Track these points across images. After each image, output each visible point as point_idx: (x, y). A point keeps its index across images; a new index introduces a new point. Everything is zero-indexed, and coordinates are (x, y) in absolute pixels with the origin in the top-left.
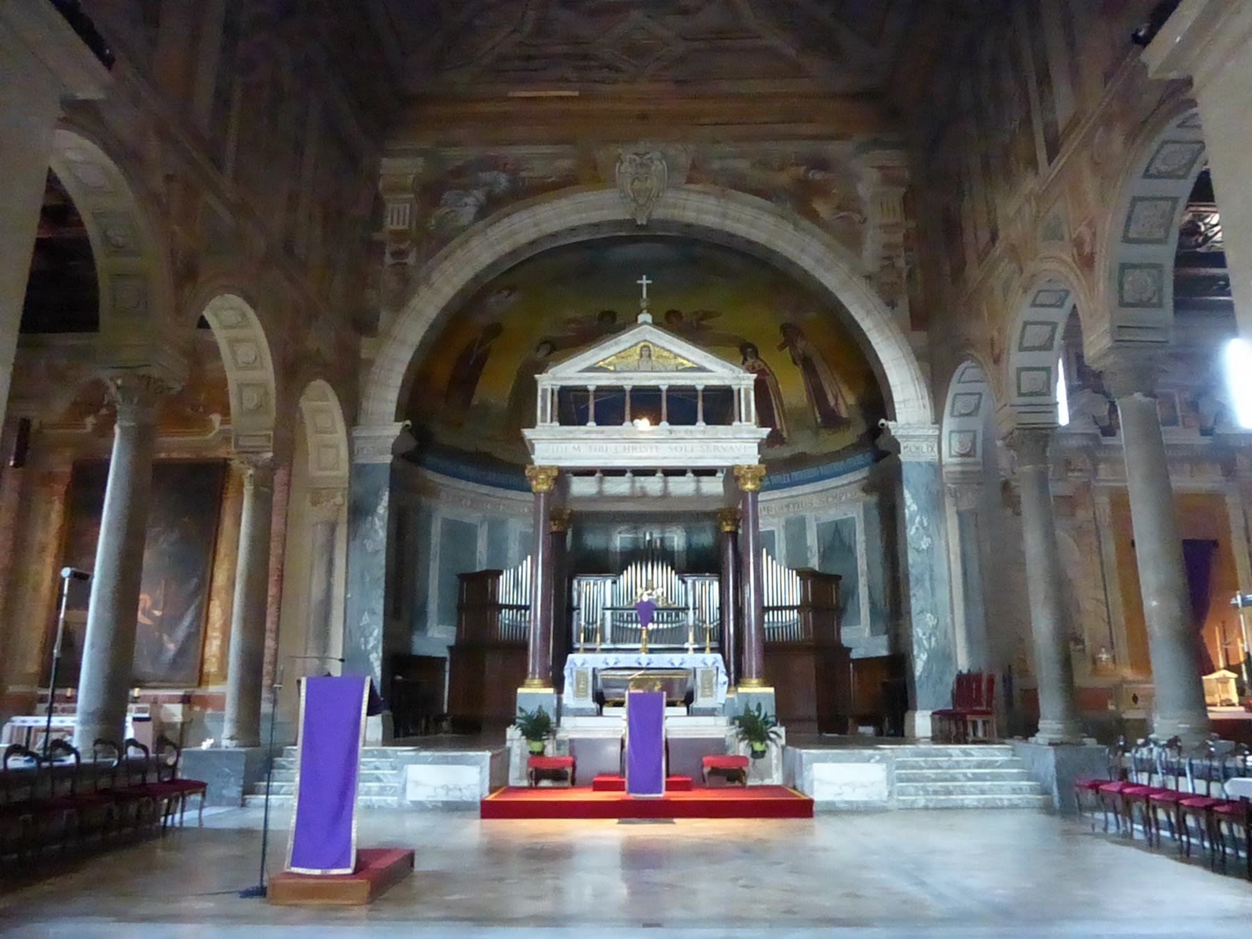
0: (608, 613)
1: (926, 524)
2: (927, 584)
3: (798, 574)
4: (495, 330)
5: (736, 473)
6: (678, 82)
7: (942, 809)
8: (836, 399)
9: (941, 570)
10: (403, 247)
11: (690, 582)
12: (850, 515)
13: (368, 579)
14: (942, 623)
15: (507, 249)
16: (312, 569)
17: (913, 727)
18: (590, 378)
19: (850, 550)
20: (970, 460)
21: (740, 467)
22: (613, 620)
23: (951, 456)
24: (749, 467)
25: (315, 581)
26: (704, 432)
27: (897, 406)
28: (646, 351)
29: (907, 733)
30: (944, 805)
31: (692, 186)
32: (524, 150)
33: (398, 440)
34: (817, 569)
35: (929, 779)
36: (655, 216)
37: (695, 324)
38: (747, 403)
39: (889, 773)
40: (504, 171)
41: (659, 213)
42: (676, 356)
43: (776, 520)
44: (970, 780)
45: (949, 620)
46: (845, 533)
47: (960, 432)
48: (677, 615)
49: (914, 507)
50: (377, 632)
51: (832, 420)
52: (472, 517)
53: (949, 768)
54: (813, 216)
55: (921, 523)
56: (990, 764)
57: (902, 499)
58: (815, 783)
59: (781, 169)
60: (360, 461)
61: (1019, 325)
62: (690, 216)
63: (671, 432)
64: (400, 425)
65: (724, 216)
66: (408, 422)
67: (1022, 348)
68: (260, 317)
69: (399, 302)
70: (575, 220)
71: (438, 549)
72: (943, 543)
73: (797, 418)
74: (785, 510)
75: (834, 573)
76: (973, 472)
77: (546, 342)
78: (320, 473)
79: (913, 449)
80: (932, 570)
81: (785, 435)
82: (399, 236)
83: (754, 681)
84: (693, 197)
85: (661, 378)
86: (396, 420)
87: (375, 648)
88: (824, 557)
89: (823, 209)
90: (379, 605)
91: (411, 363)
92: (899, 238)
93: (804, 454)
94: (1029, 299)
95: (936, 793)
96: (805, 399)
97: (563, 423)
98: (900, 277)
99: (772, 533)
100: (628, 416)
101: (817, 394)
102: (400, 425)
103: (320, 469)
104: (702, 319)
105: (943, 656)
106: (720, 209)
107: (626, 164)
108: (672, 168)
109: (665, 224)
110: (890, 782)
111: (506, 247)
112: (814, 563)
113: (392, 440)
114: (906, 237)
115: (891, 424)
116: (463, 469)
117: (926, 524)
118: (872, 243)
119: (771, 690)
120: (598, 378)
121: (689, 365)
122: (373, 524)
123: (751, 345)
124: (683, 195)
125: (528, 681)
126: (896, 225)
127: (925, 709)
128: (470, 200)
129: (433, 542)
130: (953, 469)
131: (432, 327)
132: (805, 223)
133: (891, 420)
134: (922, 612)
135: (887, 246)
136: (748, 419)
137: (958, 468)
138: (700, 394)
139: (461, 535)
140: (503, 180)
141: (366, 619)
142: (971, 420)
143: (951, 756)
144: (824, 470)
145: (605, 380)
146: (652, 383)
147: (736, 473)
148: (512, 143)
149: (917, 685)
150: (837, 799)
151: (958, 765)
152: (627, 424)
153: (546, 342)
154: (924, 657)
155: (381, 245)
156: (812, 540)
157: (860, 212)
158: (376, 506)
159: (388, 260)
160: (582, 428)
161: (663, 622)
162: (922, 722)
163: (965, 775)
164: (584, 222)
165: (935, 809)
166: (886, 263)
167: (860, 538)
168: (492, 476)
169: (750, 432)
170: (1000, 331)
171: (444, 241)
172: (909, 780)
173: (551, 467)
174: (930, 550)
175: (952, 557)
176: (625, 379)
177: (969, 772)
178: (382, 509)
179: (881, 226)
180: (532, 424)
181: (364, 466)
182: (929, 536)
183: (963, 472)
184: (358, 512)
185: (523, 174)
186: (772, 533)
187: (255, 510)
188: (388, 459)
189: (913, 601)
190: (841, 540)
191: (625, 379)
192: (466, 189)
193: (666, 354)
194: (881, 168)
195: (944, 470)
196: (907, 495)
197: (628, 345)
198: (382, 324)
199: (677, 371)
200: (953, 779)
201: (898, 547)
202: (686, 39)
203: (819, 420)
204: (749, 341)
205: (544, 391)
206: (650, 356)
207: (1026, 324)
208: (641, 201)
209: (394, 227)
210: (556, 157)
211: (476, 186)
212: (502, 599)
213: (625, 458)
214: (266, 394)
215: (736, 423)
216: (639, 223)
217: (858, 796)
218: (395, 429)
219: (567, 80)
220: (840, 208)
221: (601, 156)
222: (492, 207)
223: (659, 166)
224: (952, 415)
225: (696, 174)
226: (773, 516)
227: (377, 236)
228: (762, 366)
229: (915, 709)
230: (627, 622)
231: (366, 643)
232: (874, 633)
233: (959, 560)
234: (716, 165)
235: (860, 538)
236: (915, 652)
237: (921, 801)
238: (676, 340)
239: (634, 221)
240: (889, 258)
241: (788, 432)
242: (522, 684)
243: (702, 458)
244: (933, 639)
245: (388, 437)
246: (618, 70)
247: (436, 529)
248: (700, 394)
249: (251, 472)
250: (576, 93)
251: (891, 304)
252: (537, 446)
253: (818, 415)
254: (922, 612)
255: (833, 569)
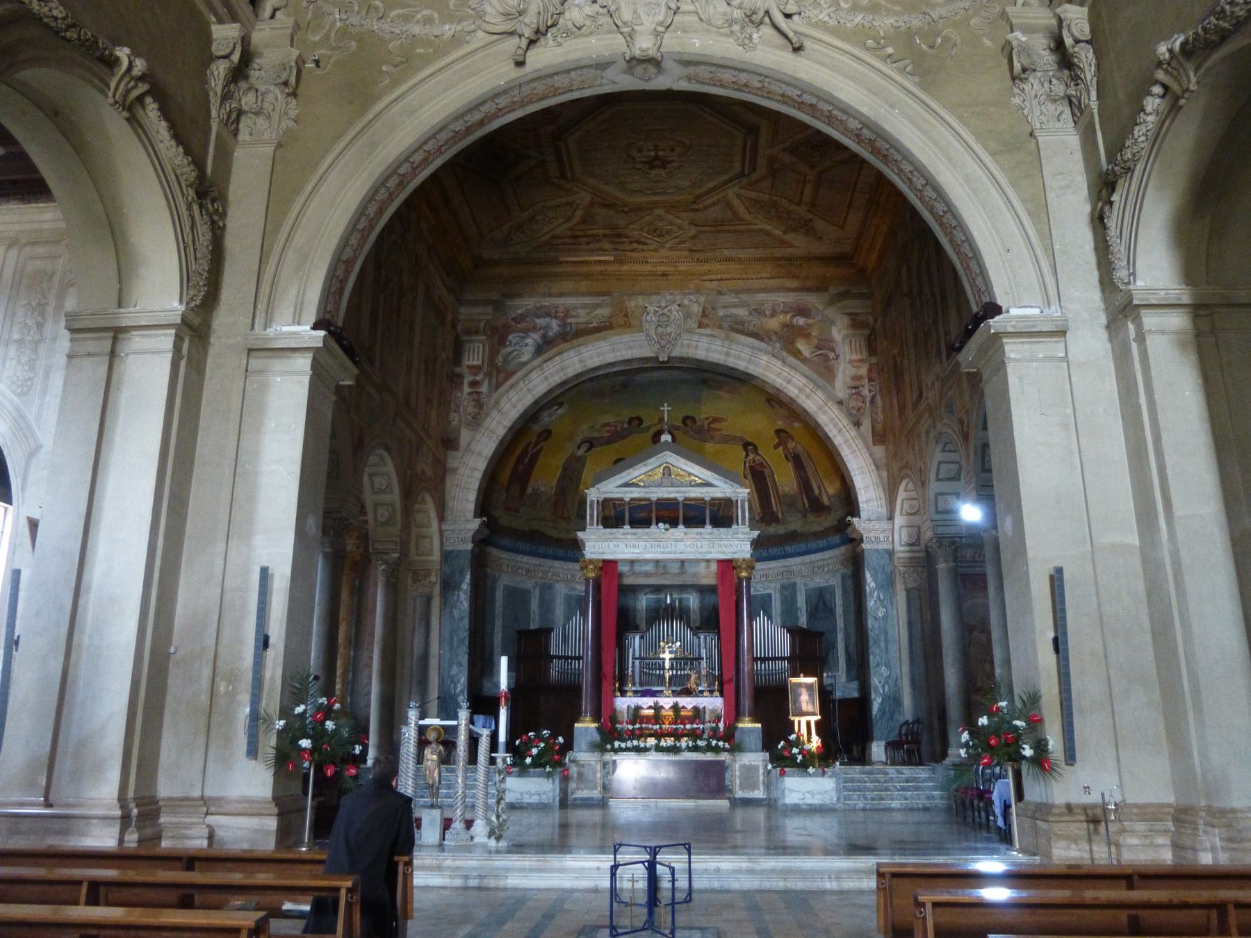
0: (637, 662)
1: (882, 597)
2: (883, 644)
3: (788, 631)
4: (547, 434)
5: (734, 564)
6: (691, 251)
7: (875, 810)
8: (819, 488)
9: (893, 633)
10: (478, 378)
11: (702, 637)
12: (831, 583)
13: (455, 639)
14: (894, 674)
15: (559, 381)
16: (413, 633)
17: (870, 754)
18: (626, 492)
19: (831, 611)
20: (914, 548)
21: (737, 560)
22: (640, 667)
23: (901, 545)
24: (744, 560)
25: (416, 640)
26: (710, 534)
27: (861, 505)
28: (667, 471)
29: (867, 758)
30: (876, 807)
31: (702, 331)
32: (570, 301)
33: (477, 532)
34: (805, 626)
35: (869, 790)
36: (673, 354)
37: (706, 427)
38: (743, 512)
39: (838, 784)
40: (556, 317)
41: (677, 352)
42: (690, 474)
43: (773, 585)
44: (899, 790)
45: (898, 671)
46: (828, 597)
47: (908, 527)
48: (692, 664)
49: (873, 585)
50: (463, 680)
51: (817, 506)
52: (528, 584)
53: (885, 782)
54: (797, 354)
55: (879, 597)
56: (915, 780)
57: (864, 577)
58: (786, 791)
59: (773, 316)
60: (448, 548)
61: (935, 463)
62: (701, 354)
63: (686, 534)
64: (478, 521)
65: (728, 354)
66: (485, 519)
67: (938, 480)
68: (392, 459)
69: (476, 422)
70: (610, 358)
71: (501, 610)
72: (895, 612)
73: (789, 503)
74: (780, 577)
75: (819, 630)
76: (919, 558)
77: (586, 442)
78: (417, 558)
79: (873, 539)
80: (886, 632)
81: (780, 515)
82: (475, 370)
83: (747, 719)
84: (704, 339)
85: (678, 492)
86: (475, 516)
87: (462, 691)
88: (812, 615)
89: (803, 346)
90: (464, 660)
91: (486, 471)
92: (863, 371)
93: (795, 531)
94: (940, 447)
95: (872, 799)
96: (795, 487)
97: (605, 527)
98: (864, 402)
99: (770, 596)
100: (654, 521)
101: (805, 484)
102: (478, 521)
103: (418, 554)
104: (712, 423)
105: (894, 701)
106: (725, 350)
107: (651, 315)
108: (687, 316)
109: (682, 359)
110: (838, 791)
111: (557, 379)
112: (803, 621)
113: (473, 532)
114: (870, 370)
115: (855, 520)
116: (521, 545)
117: (882, 597)
118: (841, 387)
119: (760, 725)
120: (631, 492)
121: (700, 481)
122: (458, 596)
123: (751, 444)
124: (696, 338)
125: (582, 718)
126: (861, 361)
127: (880, 740)
128: (529, 341)
129: (497, 605)
130: (901, 555)
131: (501, 442)
132: (791, 359)
133: (855, 516)
134: (877, 666)
135: (856, 378)
136: (744, 523)
137: (907, 555)
138: (708, 521)
139: (518, 598)
140: (555, 325)
141: (455, 670)
142: (916, 517)
143: (887, 774)
144: (812, 545)
145: (635, 493)
146: (672, 496)
147: (734, 564)
148: (561, 295)
149: (874, 722)
150: (801, 802)
151: (892, 780)
152: (653, 527)
153: (586, 442)
154: (879, 700)
155: (461, 376)
156: (801, 602)
157: (834, 351)
158: (461, 583)
159: (466, 389)
160: (621, 530)
161: (681, 670)
162: (878, 750)
163: (895, 787)
164: (620, 359)
165: (870, 810)
166: (854, 391)
167: (839, 602)
168: (542, 550)
169: (743, 533)
170: (925, 464)
171: (510, 374)
172: (854, 790)
173: (598, 560)
174: (885, 618)
175: (901, 623)
176: (652, 492)
177: (898, 785)
178: (466, 585)
179: (851, 362)
180: (583, 529)
181: (451, 552)
182: (885, 607)
183: (911, 558)
184: (448, 586)
185: (570, 320)
186: (770, 596)
187: (386, 594)
188: (470, 546)
189: (871, 657)
190: (824, 604)
191: (652, 492)
192: (526, 331)
193: (682, 473)
194: (849, 314)
195: (896, 556)
196: (868, 575)
197: (654, 466)
198: (463, 441)
199: (691, 486)
200: (887, 789)
201: (410, 923)
202: (695, 225)
203: (807, 505)
204: (749, 440)
205: (592, 502)
206: (670, 475)
207: (940, 463)
208: (663, 343)
209: (471, 363)
210: (598, 306)
211: (535, 329)
212: (553, 652)
213: (652, 553)
214: (394, 510)
215: (734, 526)
216: (661, 360)
217: (816, 800)
218: (475, 524)
219: (604, 250)
220: (818, 347)
221: (631, 304)
222: (546, 346)
223: (676, 314)
224: (901, 514)
225: (705, 319)
226: (770, 582)
227: (457, 370)
228: (762, 460)
229: (872, 740)
230: (652, 669)
231: (455, 688)
232: (849, 679)
233: (906, 625)
234: (721, 313)
235: (839, 602)
236: (873, 696)
237: (861, 805)
238: (689, 463)
239: (657, 358)
240: (856, 388)
241: (782, 514)
242: (578, 721)
243: (710, 553)
244: (886, 687)
245: (469, 530)
246: (646, 244)
247: (499, 595)
248: (708, 521)
249: (383, 567)
250: (612, 258)
251: (857, 424)
252: (587, 544)
253: (806, 501)
254: (877, 666)
255: (820, 626)
